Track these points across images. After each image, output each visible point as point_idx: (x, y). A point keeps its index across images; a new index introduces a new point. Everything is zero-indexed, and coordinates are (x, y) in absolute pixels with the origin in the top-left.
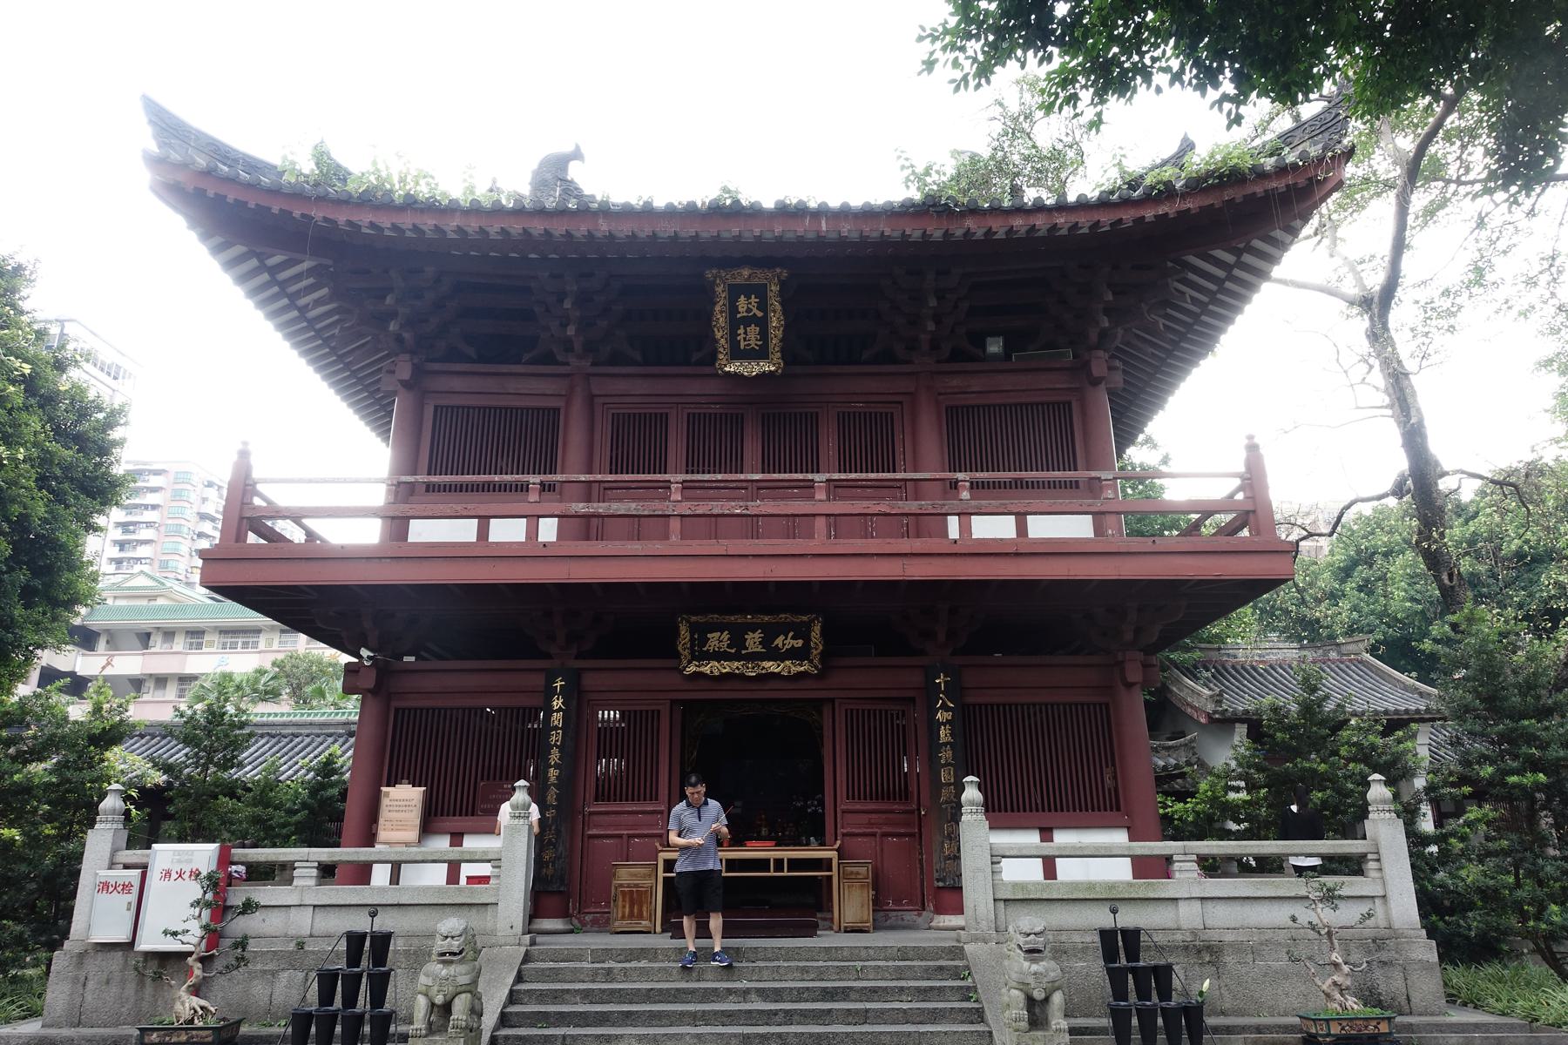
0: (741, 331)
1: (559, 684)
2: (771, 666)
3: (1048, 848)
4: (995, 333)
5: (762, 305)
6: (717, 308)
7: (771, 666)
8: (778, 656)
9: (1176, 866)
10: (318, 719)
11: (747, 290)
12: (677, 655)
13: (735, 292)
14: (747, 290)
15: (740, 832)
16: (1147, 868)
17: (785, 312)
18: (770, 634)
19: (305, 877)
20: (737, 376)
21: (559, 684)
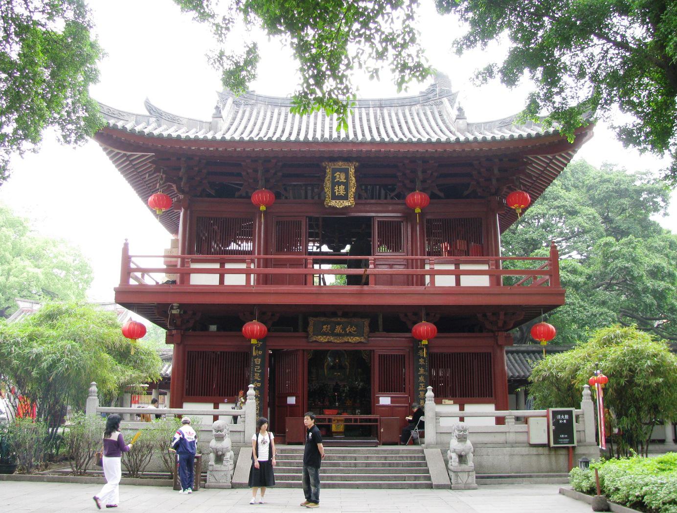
0: (336, 188)
3: (216, 412)
5: (347, 178)
6: (327, 178)
9: (506, 420)
11: (341, 170)
13: (334, 171)
15: (419, 213)
16: (500, 421)
19: (510, 422)
20: (334, 208)
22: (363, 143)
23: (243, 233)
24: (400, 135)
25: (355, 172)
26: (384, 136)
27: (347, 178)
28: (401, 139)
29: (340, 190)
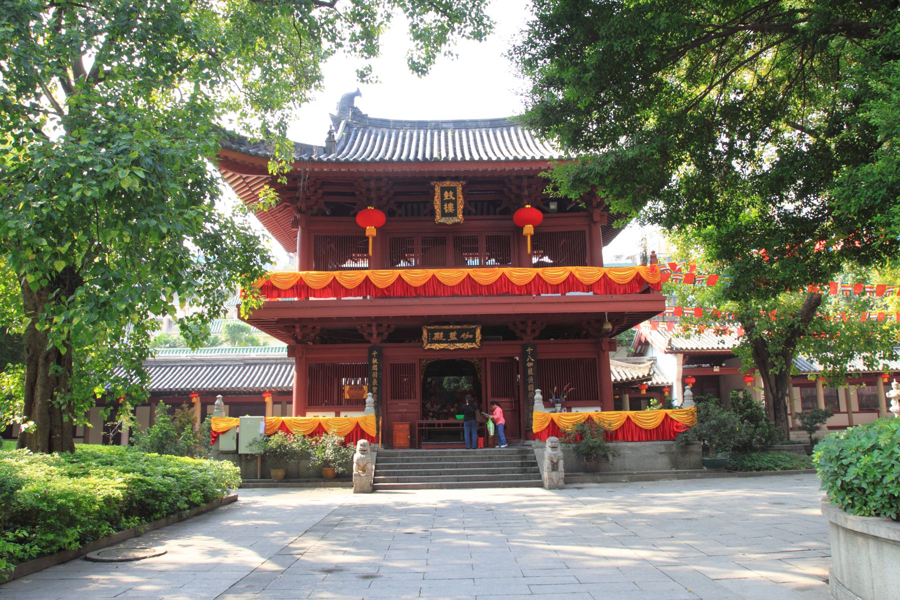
1: (375, 353)
5: (455, 195)
8: (461, 341)
11: (448, 189)
14: (448, 189)
17: (464, 198)
18: (460, 332)
21: (375, 353)
22: (437, 161)
23: (358, 251)
25: (463, 191)
27: (455, 195)
29: (449, 208)
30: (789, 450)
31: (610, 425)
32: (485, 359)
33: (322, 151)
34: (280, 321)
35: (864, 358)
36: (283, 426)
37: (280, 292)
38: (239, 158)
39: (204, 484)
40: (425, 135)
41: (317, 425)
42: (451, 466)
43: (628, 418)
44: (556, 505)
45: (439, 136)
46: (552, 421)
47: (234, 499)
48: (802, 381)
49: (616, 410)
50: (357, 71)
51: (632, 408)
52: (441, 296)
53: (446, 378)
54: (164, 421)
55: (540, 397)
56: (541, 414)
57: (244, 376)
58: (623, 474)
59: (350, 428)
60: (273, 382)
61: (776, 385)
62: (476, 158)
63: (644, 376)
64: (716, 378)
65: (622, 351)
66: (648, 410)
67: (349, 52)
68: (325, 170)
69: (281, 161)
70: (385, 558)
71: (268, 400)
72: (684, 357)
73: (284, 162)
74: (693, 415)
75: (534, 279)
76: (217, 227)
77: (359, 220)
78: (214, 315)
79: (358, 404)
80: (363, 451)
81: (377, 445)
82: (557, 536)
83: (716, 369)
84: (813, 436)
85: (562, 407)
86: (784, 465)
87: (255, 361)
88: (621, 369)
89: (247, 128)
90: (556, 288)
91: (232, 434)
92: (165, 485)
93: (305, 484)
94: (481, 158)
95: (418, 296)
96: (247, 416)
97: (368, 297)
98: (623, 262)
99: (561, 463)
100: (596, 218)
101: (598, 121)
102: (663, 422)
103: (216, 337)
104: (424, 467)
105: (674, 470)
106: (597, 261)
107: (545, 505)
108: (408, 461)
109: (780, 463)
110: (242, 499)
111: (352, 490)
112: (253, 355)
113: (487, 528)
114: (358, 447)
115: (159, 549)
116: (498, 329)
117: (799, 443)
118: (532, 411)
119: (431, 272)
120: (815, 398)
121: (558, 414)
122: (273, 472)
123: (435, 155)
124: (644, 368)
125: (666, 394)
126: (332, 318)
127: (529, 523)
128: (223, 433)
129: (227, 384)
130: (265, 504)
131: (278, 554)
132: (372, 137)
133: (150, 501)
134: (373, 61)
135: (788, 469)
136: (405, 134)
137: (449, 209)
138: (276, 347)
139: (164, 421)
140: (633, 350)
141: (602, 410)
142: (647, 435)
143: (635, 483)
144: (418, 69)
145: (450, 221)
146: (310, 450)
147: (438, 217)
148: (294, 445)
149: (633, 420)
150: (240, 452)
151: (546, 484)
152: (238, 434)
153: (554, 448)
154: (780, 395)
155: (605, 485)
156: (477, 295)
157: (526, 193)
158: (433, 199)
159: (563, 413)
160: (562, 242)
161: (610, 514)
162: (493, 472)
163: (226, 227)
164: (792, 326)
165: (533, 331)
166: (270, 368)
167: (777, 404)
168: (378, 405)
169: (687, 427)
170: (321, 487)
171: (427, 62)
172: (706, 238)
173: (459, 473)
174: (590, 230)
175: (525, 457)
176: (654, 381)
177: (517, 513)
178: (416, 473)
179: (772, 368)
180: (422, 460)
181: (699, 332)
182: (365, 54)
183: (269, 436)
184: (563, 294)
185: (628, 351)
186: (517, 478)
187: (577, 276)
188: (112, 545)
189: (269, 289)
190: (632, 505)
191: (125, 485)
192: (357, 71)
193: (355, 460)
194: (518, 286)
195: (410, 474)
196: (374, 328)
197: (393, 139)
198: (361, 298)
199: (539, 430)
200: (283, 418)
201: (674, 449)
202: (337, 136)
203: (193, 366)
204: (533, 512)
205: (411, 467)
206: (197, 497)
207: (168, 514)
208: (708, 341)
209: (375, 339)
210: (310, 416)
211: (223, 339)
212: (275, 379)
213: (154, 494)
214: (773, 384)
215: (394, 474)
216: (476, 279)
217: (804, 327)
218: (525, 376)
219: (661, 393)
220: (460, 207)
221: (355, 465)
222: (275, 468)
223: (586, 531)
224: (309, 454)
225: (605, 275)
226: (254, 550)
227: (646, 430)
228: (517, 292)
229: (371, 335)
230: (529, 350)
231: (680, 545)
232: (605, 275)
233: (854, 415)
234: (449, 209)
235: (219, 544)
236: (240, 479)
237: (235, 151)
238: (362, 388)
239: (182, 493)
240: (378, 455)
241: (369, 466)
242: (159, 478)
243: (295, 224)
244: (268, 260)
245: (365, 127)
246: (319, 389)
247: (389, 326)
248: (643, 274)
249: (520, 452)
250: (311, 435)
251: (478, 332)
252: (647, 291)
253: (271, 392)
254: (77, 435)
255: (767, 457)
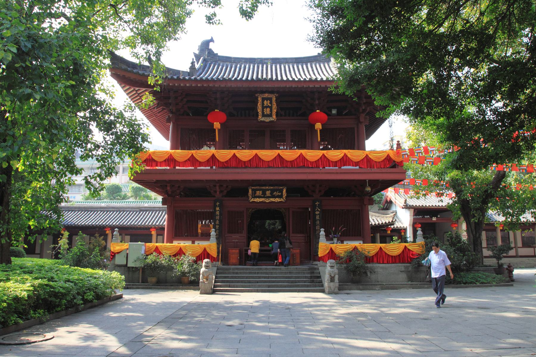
1: (218, 204)
2: (272, 200)
4: (334, 108)
5: (271, 103)
7: (272, 200)
8: (274, 197)
10: (103, 205)
11: (267, 99)
12: (248, 197)
14: (267, 99)
17: (277, 105)
18: (272, 191)
20: (264, 122)
21: (218, 204)
24: (299, 77)
25: (276, 100)
26: (294, 77)
27: (271, 103)
28: (300, 79)
30: (484, 271)
31: (369, 252)
32: (289, 208)
33: (187, 74)
34: (157, 182)
35: (532, 213)
36: (157, 250)
37: (157, 163)
38: (132, 77)
39: (96, 287)
40: (254, 67)
41: (179, 249)
42: (265, 277)
43: (381, 248)
44: (333, 306)
45: (263, 67)
46: (331, 249)
47: (120, 297)
48: (492, 227)
49: (372, 243)
50: (206, 16)
51: (381, 242)
52: (261, 167)
53: (268, 221)
54: (81, 245)
55: (324, 233)
56: (324, 245)
57: (139, 218)
58: (377, 285)
59: (200, 251)
60: (157, 222)
61: (475, 228)
62: (285, 78)
63: (389, 222)
64: (434, 224)
65: (375, 207)
66: (392, 243)
67: (201, 3)
68: (188, 85)
69: (156, 76)
70: (207, 346)
71: (154, 233)
72: (414, 211)
73: (158, 77)
74: (423, 247)
75: (321, 158)
76: (112, 118)
77: (210, 118)
78: (108, 175)
79: (206, 236)
80: (206, 267)
81: (217, 263)
82: (332, 330)
83: (434, 219)
84: (501, 262)
85: (338, 240)
86: (482, 280)
87: (146, 209)
88: (375, 218)
89: (136, 55)
90: (335, 164)
91: (124, 254)
92: (64, 288)
93: (169, 287)
94: (288, 79)
95: (246, 167)
96: (139, 243)
97: (214, 167)
98: (379, 149)
99: (337, 277)
100: (362, 119)
101: (368, 43)
102: (403, 251)
103: (126, 194)
104: (247, 277)
105: (410, 283)
106: (362, 147)
107: (325, 306)
108: (237, 273)
109: (479, 279)
110: (126, 297)
111: (199, 292)
112: (146, 205)
113: (284, 323)
114: (204, 264)
115: (49, 335)
116: (298, 189)
117: (490, 266)
118: (318, 243)
119: (255, 152)
120: (495, 239)
121: (335, 245)
122: (149, 279)
123: (260, 77)
124: (389, 217)
125: (403, 234)
126: (190, 180)
127: (313, 319)
128: (118, 253)
129: (128, 222)
130: (139, 301)
131: (132, 341)
132: (220, 67)
133: (53, 299)
134: (217, 9)
135: (484, 283)
136: (241, 66)
137: (267, 112)
138: (156, 199)
139: (81, 245)
140: (382, 206)
141: (364, 243)
142: (392, 260)
143: (384, 291)
144: (247, 14)
145: (267, 120)
146: (173, 265)
147: (260, 117)
148: (163, 262)
149: (383, 249)
150: (128, 266)
151: (327, 290)
152: (127, 254)
153: (332, 267)
154: (478, 235)
155: (365, 291)
156: (284, 167)
157: (317, 102)
158: (257, 105)
159: (338, 244)
160: (340, 137)
161: (370, 313)
162: (292, 282)
163: (118, 118)
164: (486, 191)
165: (320, 191)
166: (155, 213)
167: (475, 240)
168: (220, 238)
169: (419, 255)
170: (179, 289)
171: (252, 10)
172: (439, 128)
173: (269, 282)
174: (358, 128)
175: (313, 272)
176: (395, 226)
177: (306, 310)
178: (242, 282)
179: (473, 218)
180: (246, 273)
181: (425, 195)
182: (212, 5)
183: (147, 255)
184: (340, 168)
185: (379, 207)
186: (308, 286)
187: (349, 156)
188: (18, 331)
189: (150, 160)
190: (384, 307)
191: (32, 288)
192: (206, 16)
193: (201, 272)
194: (310, 162)
195: (238, 282)
196: (217, 188)
197: (233, 69)
198: (209, 168)
199: (322, 255)
200: (157, 244)
201: (410, 269)
202: (197, 66)
203: (108, 211)
204: (317, 310)
205: (239, 277)
206: (90, 296)
207: (67, 308)
208: (431, 201)
209: (218, 195)
210: (176, 243)
211: (130, 195)
212: (158, 220)
213: (56, 295)
214: (473, 228)
215: (227, 282)
216: (283, 157)
217: (494, 192)
218: (315, 220)
219: (400, 233)
220: (274, 111)
221: (201, 275)
222: (151, 276)
223: (353, 327)
224: (173, 268)
225: (367, 156)
226: (116, 337)
227: (392, 256)
228: (310, 166)
229: (216, 192)
230: (317, 203)
231: (422, 340)
232: (367, 156)
233: (519, 249)
234: (267, 112)
235: (95, 331)
236: (124, 283)
237: (130, 72)
238: (209, 226)
239: (78, 294)
240: (218, 269)
241: (210, 276)
242: (62, 284)
243: (169, 121)
244: (147, 141)
245: (216, 62)
246: (183, 225)
247: (227, 187)
248: (392, 156)
249: (309, 269)
250: (175, 256)
251: (285, 191)
252: (394, 167)
253: (155, 228)
254: (36, 252)
255: (471, 275)
